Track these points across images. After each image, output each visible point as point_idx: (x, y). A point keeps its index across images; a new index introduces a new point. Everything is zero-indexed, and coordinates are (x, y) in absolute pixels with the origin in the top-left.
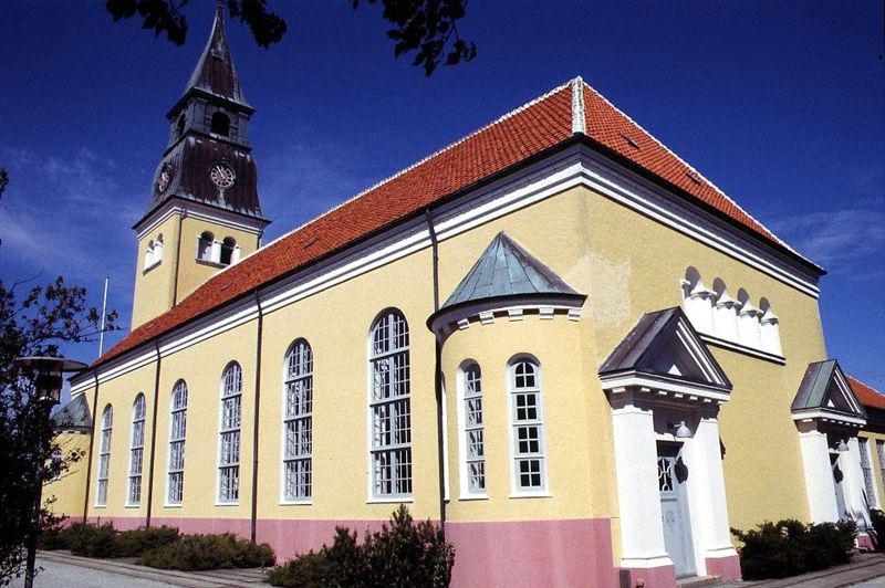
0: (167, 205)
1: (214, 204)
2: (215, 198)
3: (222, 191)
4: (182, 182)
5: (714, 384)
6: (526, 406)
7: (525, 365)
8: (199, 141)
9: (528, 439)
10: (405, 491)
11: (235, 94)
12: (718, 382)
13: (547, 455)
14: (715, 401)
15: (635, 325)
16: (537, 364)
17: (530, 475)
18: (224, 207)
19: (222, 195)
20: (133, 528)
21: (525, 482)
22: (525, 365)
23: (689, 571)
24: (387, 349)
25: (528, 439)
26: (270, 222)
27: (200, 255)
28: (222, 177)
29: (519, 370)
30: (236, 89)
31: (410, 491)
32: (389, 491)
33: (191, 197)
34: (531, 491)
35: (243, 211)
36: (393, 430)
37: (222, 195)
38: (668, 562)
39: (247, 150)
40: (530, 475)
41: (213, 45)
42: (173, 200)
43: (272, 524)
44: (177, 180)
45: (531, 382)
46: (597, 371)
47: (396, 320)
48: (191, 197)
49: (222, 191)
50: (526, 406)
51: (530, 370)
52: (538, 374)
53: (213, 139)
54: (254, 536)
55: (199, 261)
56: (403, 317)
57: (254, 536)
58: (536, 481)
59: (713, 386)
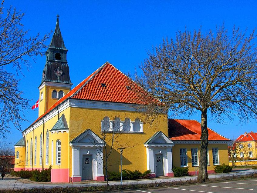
7: (59, 142)
11: (62, 46)
35: (65, 82)
48: (49, 81)
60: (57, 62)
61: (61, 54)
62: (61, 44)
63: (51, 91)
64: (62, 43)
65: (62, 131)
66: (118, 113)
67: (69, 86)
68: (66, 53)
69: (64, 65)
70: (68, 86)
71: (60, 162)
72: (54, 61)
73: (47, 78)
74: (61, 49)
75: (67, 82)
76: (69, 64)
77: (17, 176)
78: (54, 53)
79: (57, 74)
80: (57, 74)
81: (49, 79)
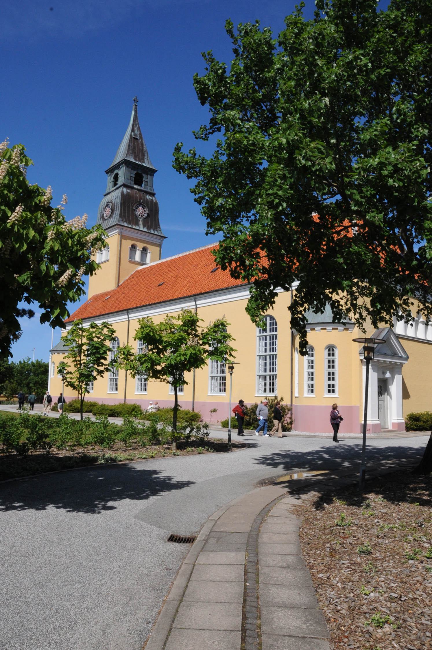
0: (112, 228)
1: (137, 228)
2: (137, 224)
3: (141, 220)
4: (121, 216)
5: (402, 357)
6: (331, 364)
7: (331, 349)
8: (129, 191)
9: (331, 376)
10: (223, 391)
11: (146, 160)
12: (403, 356)
13: (337, 382)
14: (401, 363)
15: (373, 333)
16: (336, 348)
17: (331, 389)
18: (142, 229)
19: (141, 223)
20: (117, 403)
21: (329, 391)
22: (331, 349)
23: (387, 427)
24: (266, 332)
25: (331, 376)
26: (166, 238)
27: (130, 258)
28: (140, 211)
29: (329, 350)
30: (146, 157)
31: (225, 391)
32: (265, 391)
33: (126, 224)
34: (331, 395)
35: (152, 232)
36: (268, 367)
37: (141, 223)
38: (378, 422)
39: (153, 195)
40: (331, 389)
41: (133, 130)
42: (116, 226)
43: (204, 404)
44: (117, 213)
45: (333, 355)
46: (358, 352)
47: (271, 320)
48: (126, 224)
49: (141, 220)
50: (331, 364)
51: (333, 350)
52: (336, 352)
53: (135, 189)
54: (193, 409)
55: (131, 262)
56: (274, 319)
57: (193, 409)
58: (333, 391)
59: (401, 358)
60: (138, 189)
61: (144, 176)
62: (143, 155)
63: (127, 244)
64: (146, 155)
65: (329, 328)
66: (189, 305)
67: (160, 241)
68: (153, 175)
69: (151, 198)
70: (157, 241)
71: (333, 391)
72: (133, 188)
73: (121, 219)
74: (144, 164)
75: (156, 233)
76: (158, 198)
77: (231, 422)
78: (132, 171)
79: (138, 213)
80: (138, 213)
81: (126, 222)
